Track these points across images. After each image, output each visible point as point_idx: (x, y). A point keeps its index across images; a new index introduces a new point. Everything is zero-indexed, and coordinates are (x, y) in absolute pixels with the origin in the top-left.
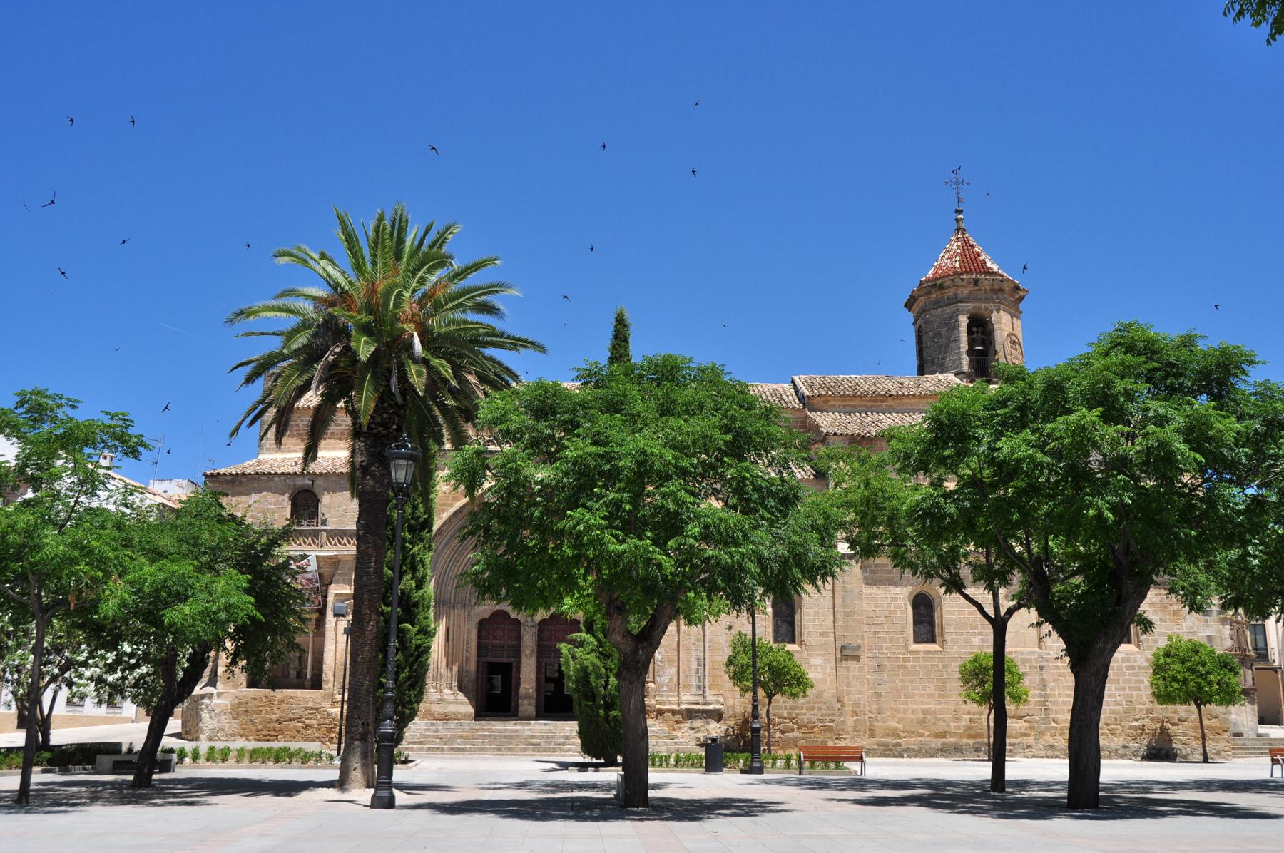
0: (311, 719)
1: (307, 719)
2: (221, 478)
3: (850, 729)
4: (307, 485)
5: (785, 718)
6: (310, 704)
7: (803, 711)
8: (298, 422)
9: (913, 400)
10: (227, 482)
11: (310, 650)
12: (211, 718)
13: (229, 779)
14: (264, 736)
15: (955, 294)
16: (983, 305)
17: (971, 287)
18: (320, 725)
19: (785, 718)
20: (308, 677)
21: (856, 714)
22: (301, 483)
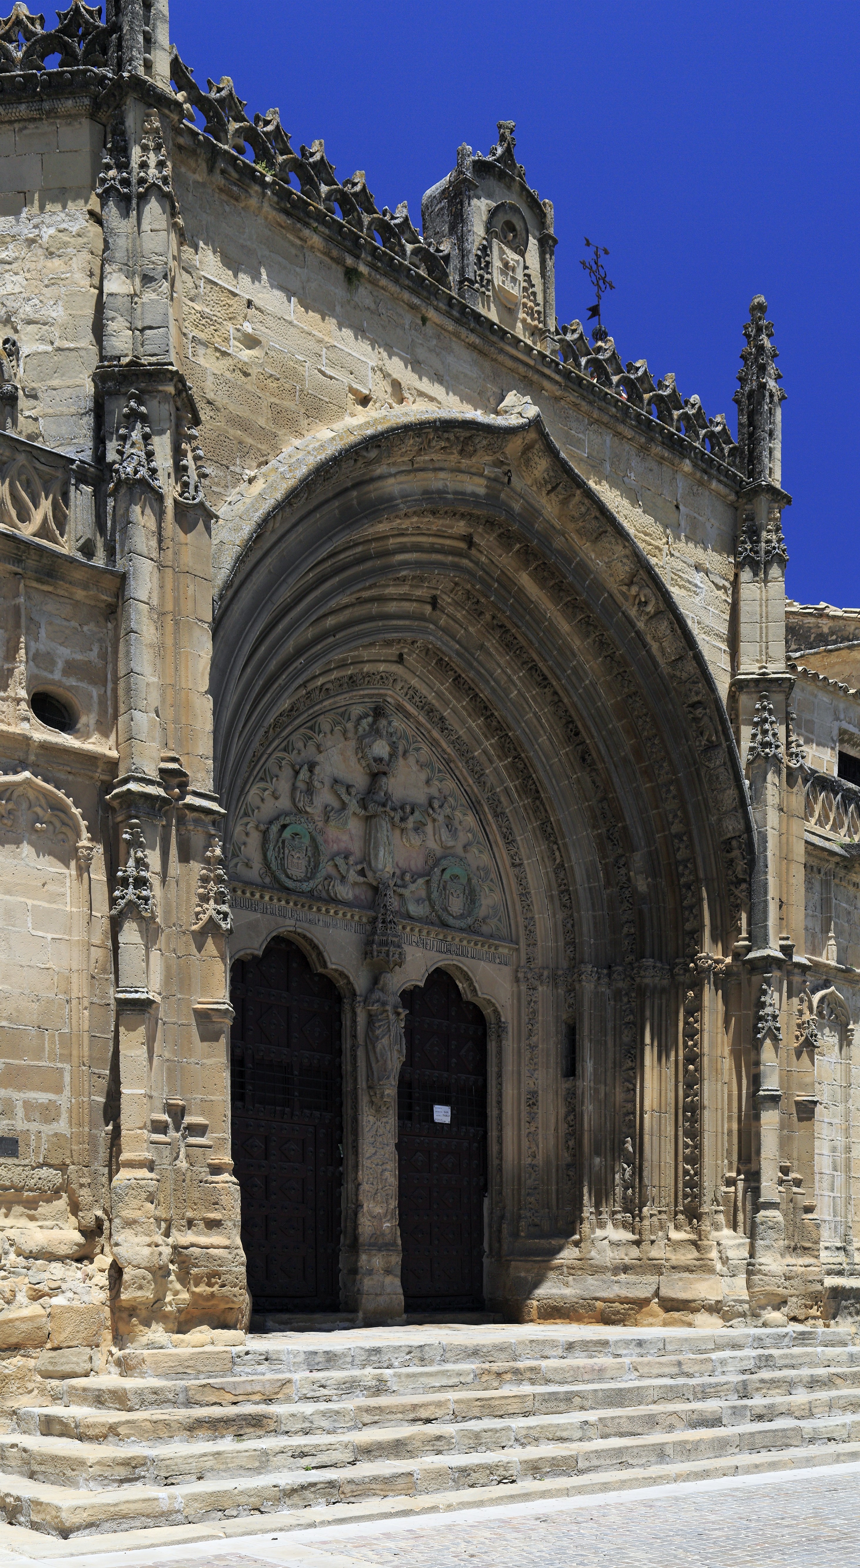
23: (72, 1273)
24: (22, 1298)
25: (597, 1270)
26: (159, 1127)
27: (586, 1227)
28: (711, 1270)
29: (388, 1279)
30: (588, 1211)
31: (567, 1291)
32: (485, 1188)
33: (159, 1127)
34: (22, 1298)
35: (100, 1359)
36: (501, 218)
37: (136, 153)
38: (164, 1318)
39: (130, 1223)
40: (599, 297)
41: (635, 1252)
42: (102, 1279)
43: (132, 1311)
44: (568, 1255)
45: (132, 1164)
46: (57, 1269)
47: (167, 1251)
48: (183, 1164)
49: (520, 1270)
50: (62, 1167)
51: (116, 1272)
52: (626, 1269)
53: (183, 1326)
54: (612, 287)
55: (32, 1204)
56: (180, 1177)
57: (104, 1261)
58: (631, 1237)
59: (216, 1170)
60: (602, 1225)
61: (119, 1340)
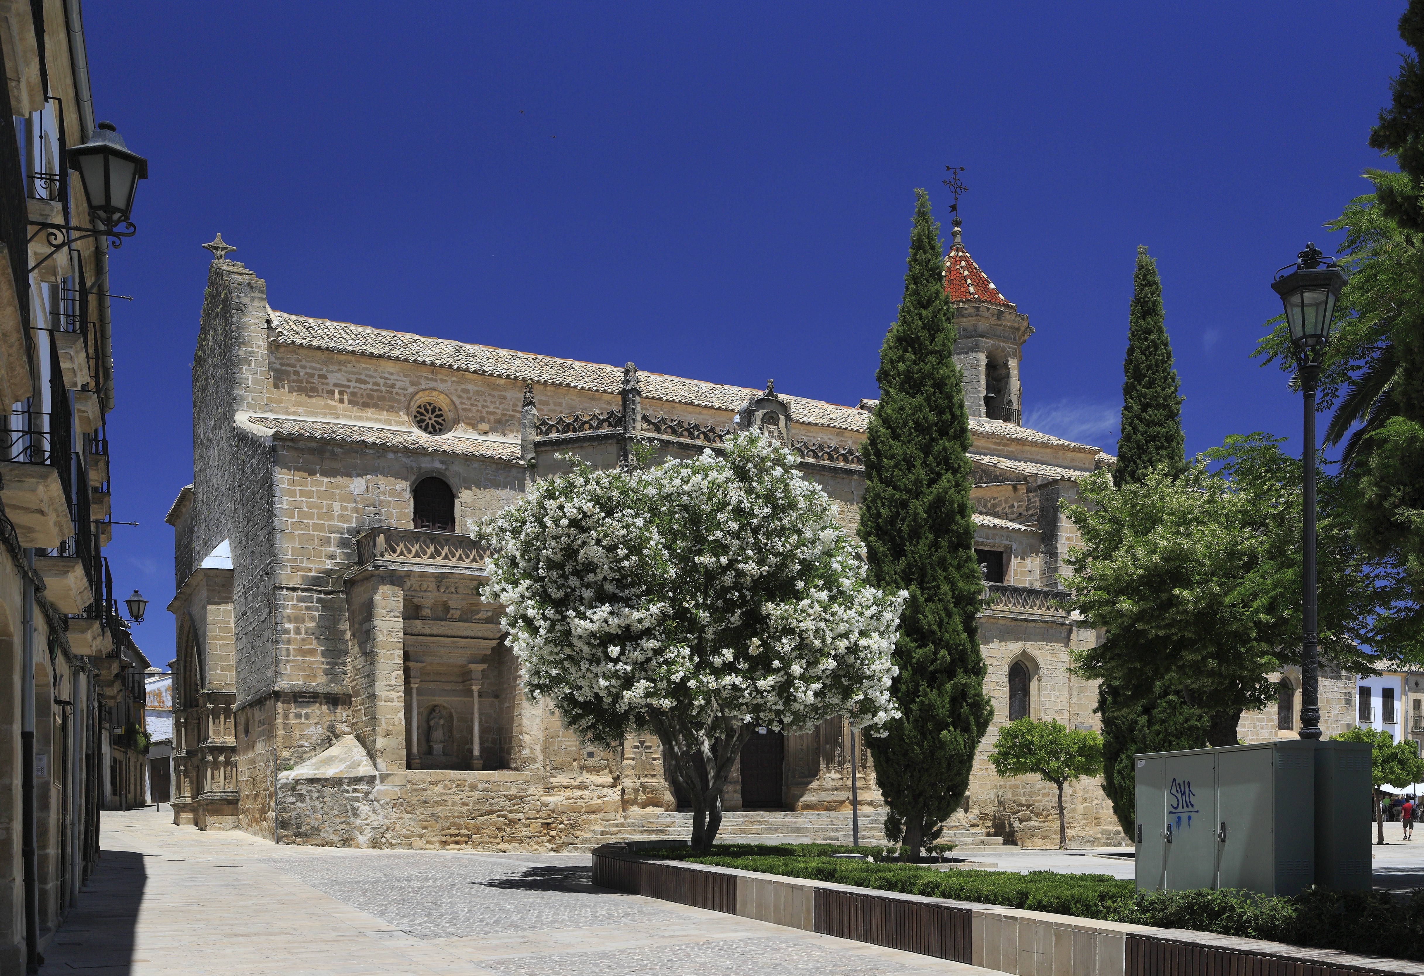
0: (516, 812)
1: (510, 812)
2: (301, 444)
3: (1080, 817)
4: (437, 470)
5: (1023, 805)
6: (514, 792)
7: (1039, 798)
8: (298, 368)
9: (1034, 449)
10: (312, 451)
11: (476, 715)
12: (374, 811)
13: (590, 893)
14: (452, 835)
15: (975, 326)
16: (1002, 344)
17: (994, 321)
18: (528, 819)
19: (1023, 805)
20: (476, 752)
21: (1085, 800)
22: (429, 466)
23: (610, 791)
24: (595, 798)
25: (825, 790)
26: (637, 747)
27: (821, 773)
28: (870, 789)
29: (735, 795)
30: (823, 766)
31: (813, 799)
32: (783, 759)
33: (637, 747)
34: (595, 798)
35: (618, 816)
36: (767, 416)
37: (630, 456)
38: (638, 804)
39: (627, 776)
40: (956, 199)
41: (841, 782)
42: (619, 793)
43: (628, 802)
44: (814, 784)
45: (627, 759)
46: (605, 790)
47: (638, 784)
48: (644, 758)
49: (795, 791)
50: (607, 760)
51: (623, 791)
52: (837, 789)
53: (644, 805)
54: (966, 190)
55: (598, 771)
56: (643, 762)
57: (620, 787)
58: (840, 776)
59: (654, 759)
60: (830, 772)
61: (624, 810)
